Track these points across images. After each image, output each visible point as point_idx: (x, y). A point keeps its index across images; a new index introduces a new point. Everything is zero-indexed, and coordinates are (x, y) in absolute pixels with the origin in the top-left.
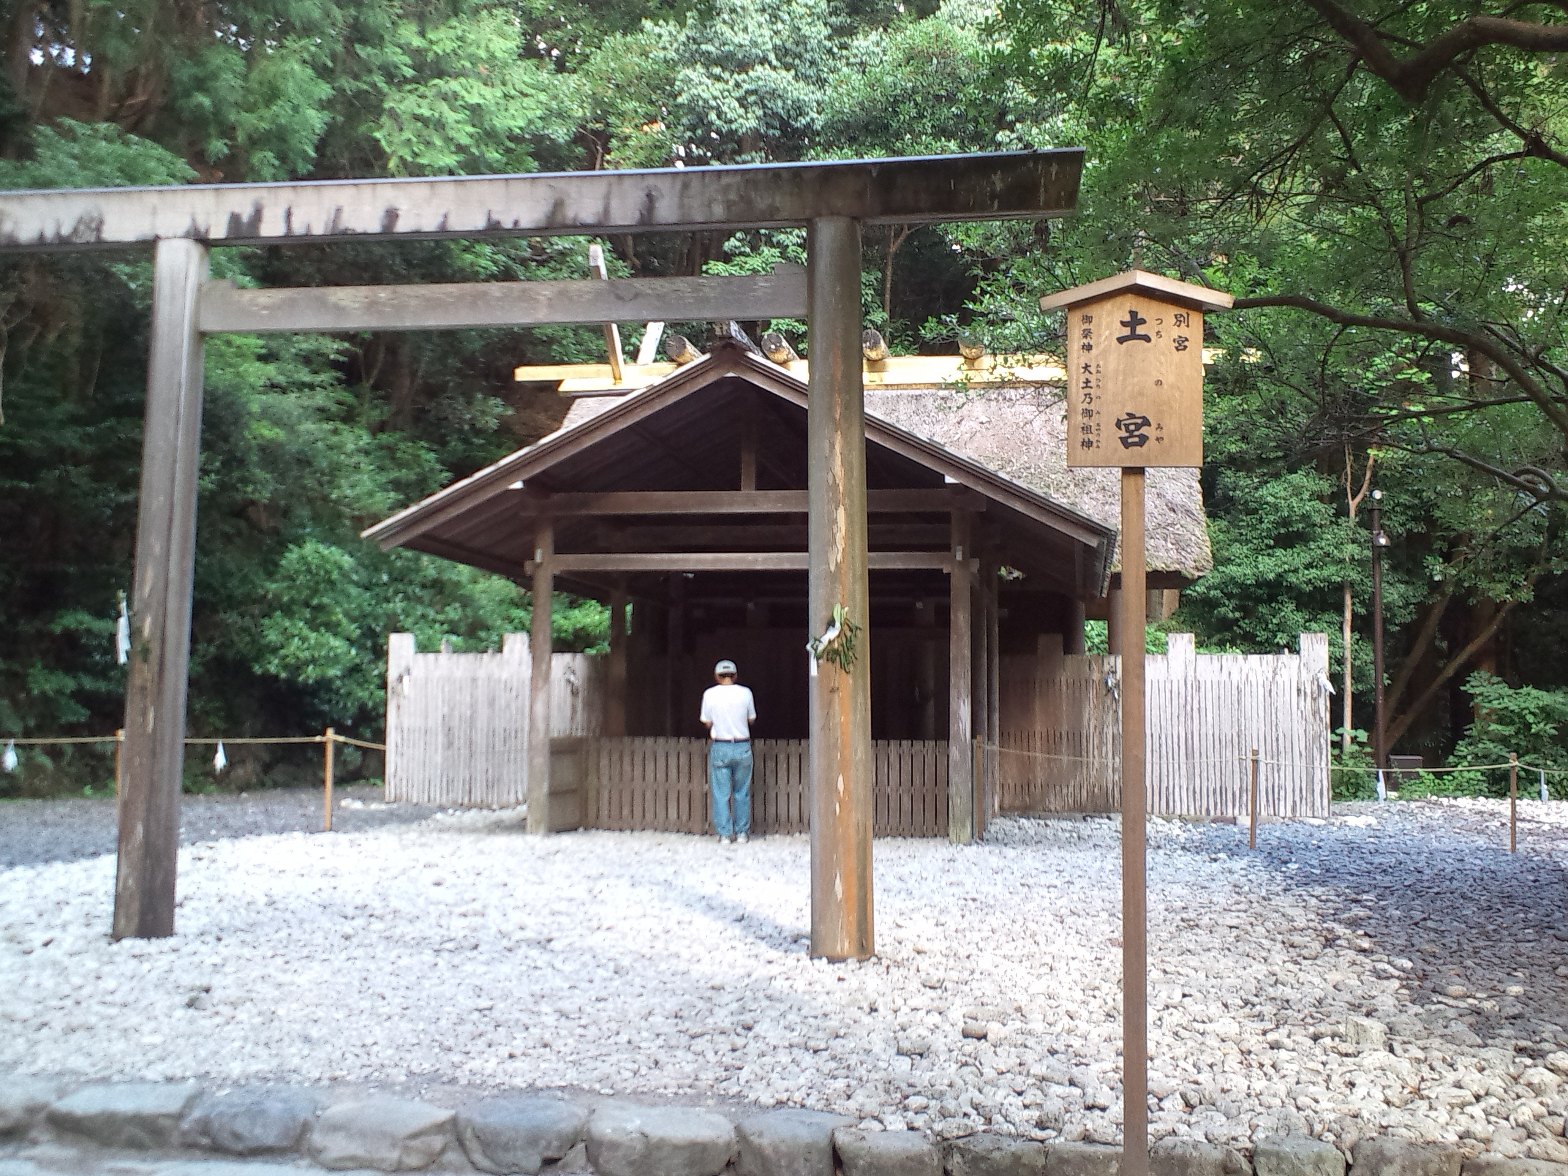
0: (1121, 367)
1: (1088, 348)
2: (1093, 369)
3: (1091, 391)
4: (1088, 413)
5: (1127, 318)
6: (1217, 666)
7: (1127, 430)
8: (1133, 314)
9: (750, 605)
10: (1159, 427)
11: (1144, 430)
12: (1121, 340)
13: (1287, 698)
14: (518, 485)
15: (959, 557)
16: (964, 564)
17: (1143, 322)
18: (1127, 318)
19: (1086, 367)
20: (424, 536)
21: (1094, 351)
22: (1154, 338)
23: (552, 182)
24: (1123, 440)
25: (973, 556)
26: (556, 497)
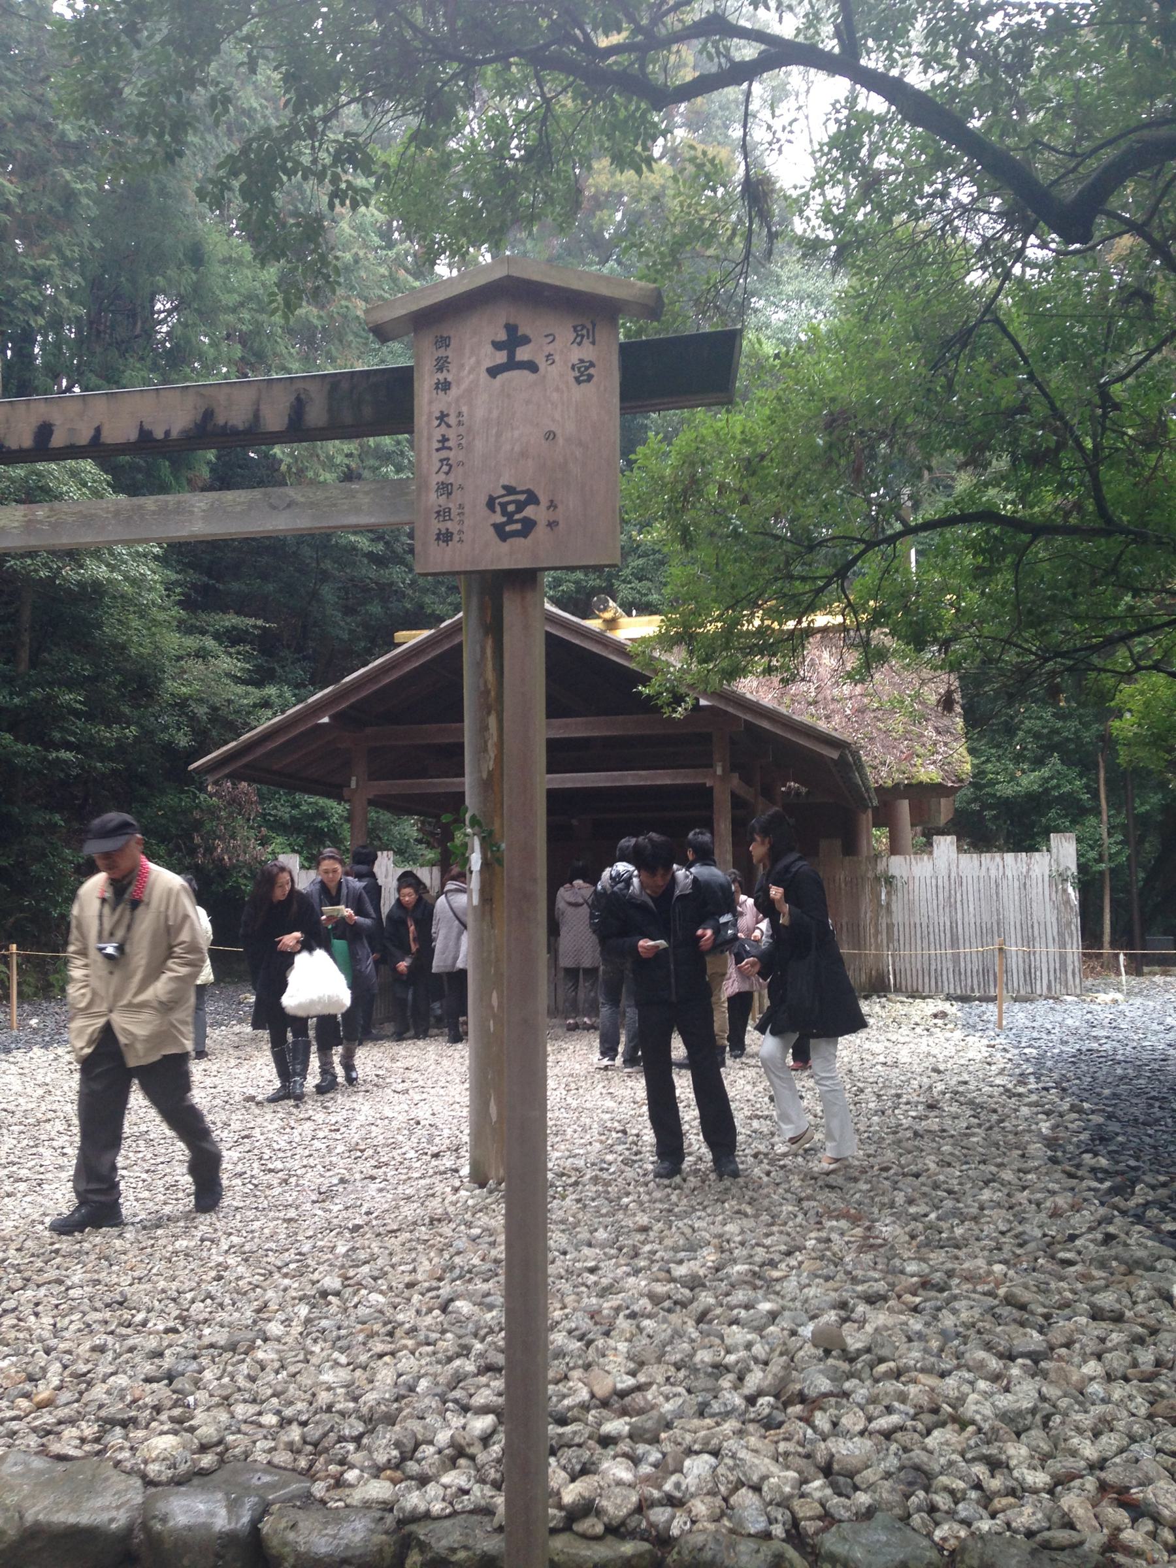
0: (495, 414)
1: (445, 386)
2: (452, 420)
3: (451, 454)
4: (445, 489)
5: (502, 336)
6: (976, 863)
7: (504, 512)
8: (511, 329)
9: (575, 822)
10: (552, 505)
11: (529, 511)
12: (493, 372)
13: (1040, 891)
14: (326, 720)
15: (719, 771)
16: (724, 779)
17: (526, 340)
18: (502, 336)
19: (442, 417)
20: (246, 766)
21: (454, 392)
22: (542, 365)
23: (203, 391)
24: (500, 530)
25: (732, 770)
26: (369, 731)
